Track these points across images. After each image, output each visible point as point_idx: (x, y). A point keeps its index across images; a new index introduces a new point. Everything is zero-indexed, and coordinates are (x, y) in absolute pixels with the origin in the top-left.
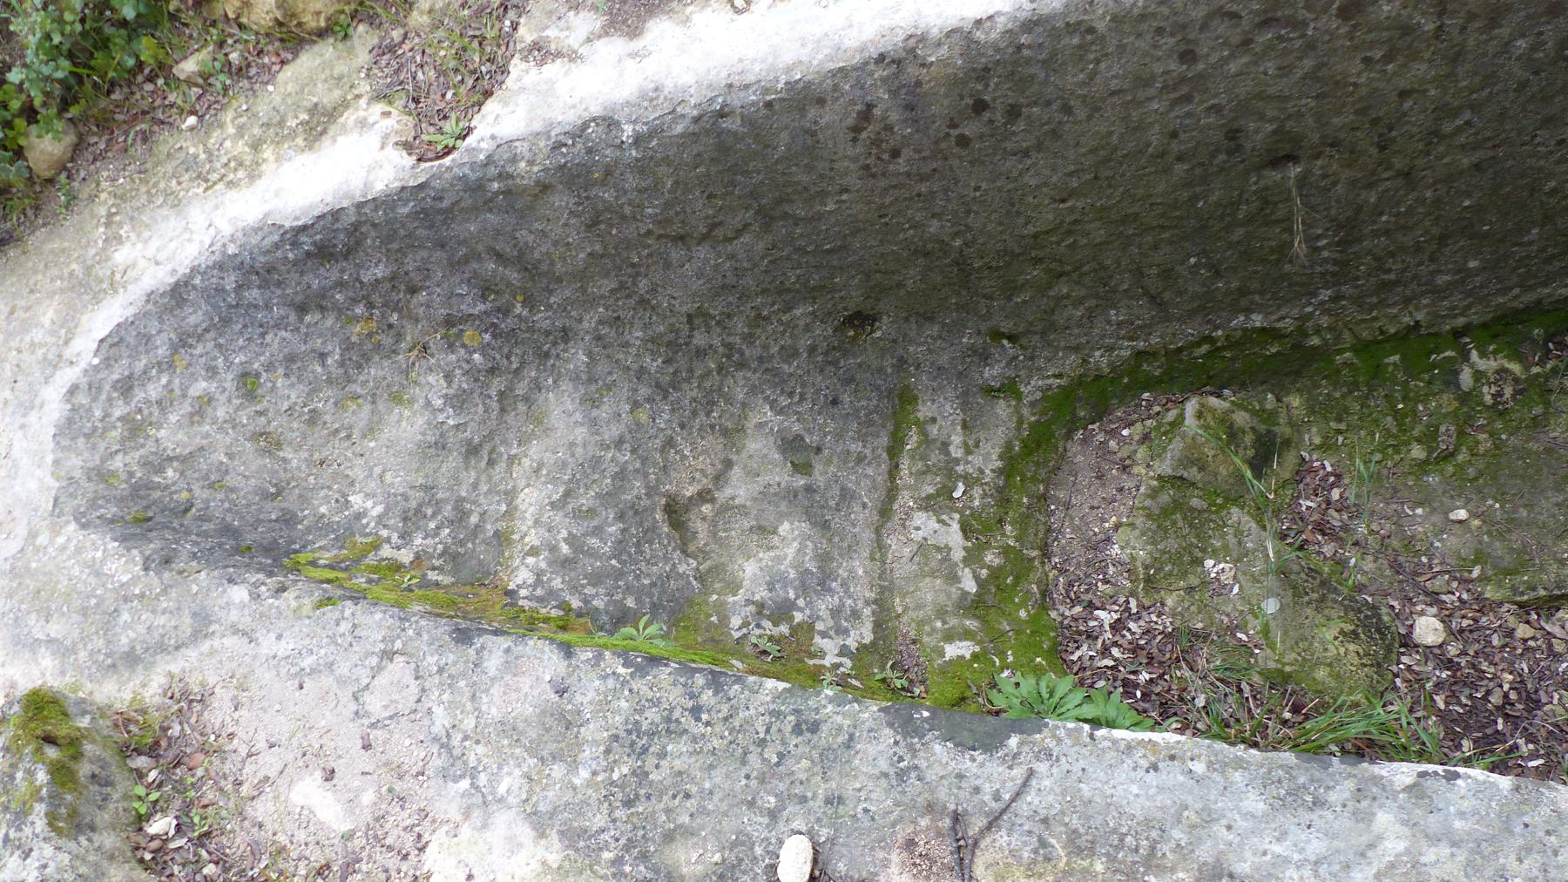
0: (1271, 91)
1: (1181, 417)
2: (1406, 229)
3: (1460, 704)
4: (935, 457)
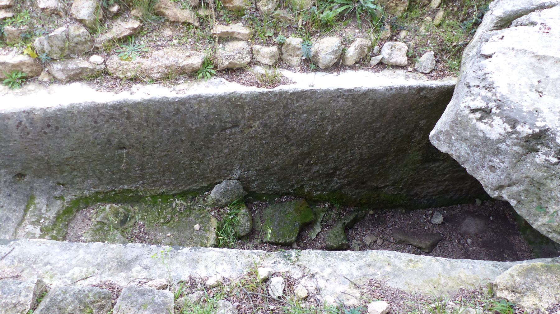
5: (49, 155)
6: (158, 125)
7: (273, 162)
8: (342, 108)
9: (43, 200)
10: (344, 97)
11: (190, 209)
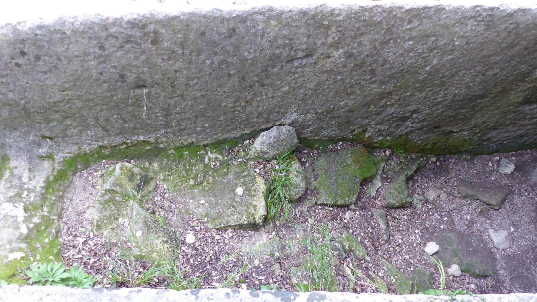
0: (133, 64)
1: (115, 169)
2: (185, 113)
3: (197, 261)
4: (16, 182)
5: (26, 97)
6: (199, 52)
7: (342, 103)
9: (23, 163)
11: (226, 164)
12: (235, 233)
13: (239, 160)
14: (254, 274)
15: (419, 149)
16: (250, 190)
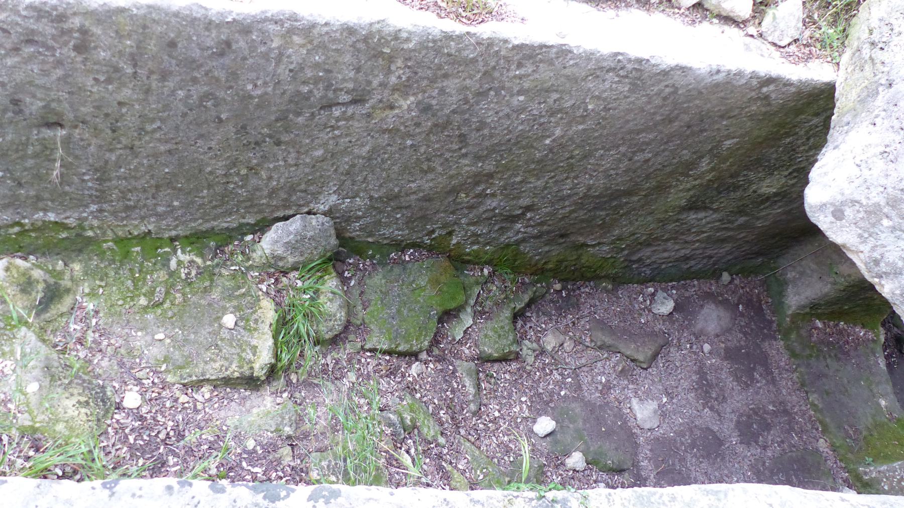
0: (37, 82)
2: (136, 178)
6: (164, 76)
7: (413, 185)
8: (605, 95)
10: (622, 73)
11: (209, 274)
12: (216, 393)
13: (233, 268)
14: (244, 464)
15: (535, 268)
16: (248, 320)
